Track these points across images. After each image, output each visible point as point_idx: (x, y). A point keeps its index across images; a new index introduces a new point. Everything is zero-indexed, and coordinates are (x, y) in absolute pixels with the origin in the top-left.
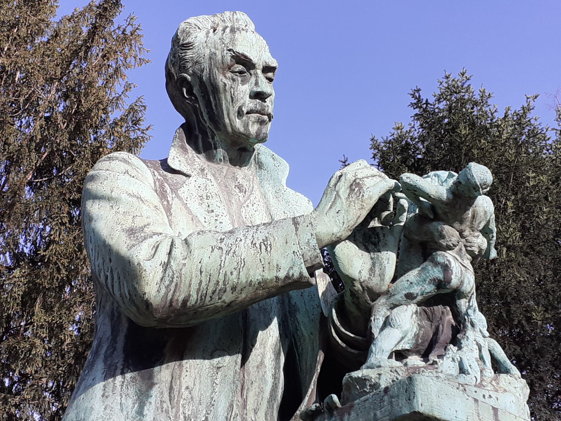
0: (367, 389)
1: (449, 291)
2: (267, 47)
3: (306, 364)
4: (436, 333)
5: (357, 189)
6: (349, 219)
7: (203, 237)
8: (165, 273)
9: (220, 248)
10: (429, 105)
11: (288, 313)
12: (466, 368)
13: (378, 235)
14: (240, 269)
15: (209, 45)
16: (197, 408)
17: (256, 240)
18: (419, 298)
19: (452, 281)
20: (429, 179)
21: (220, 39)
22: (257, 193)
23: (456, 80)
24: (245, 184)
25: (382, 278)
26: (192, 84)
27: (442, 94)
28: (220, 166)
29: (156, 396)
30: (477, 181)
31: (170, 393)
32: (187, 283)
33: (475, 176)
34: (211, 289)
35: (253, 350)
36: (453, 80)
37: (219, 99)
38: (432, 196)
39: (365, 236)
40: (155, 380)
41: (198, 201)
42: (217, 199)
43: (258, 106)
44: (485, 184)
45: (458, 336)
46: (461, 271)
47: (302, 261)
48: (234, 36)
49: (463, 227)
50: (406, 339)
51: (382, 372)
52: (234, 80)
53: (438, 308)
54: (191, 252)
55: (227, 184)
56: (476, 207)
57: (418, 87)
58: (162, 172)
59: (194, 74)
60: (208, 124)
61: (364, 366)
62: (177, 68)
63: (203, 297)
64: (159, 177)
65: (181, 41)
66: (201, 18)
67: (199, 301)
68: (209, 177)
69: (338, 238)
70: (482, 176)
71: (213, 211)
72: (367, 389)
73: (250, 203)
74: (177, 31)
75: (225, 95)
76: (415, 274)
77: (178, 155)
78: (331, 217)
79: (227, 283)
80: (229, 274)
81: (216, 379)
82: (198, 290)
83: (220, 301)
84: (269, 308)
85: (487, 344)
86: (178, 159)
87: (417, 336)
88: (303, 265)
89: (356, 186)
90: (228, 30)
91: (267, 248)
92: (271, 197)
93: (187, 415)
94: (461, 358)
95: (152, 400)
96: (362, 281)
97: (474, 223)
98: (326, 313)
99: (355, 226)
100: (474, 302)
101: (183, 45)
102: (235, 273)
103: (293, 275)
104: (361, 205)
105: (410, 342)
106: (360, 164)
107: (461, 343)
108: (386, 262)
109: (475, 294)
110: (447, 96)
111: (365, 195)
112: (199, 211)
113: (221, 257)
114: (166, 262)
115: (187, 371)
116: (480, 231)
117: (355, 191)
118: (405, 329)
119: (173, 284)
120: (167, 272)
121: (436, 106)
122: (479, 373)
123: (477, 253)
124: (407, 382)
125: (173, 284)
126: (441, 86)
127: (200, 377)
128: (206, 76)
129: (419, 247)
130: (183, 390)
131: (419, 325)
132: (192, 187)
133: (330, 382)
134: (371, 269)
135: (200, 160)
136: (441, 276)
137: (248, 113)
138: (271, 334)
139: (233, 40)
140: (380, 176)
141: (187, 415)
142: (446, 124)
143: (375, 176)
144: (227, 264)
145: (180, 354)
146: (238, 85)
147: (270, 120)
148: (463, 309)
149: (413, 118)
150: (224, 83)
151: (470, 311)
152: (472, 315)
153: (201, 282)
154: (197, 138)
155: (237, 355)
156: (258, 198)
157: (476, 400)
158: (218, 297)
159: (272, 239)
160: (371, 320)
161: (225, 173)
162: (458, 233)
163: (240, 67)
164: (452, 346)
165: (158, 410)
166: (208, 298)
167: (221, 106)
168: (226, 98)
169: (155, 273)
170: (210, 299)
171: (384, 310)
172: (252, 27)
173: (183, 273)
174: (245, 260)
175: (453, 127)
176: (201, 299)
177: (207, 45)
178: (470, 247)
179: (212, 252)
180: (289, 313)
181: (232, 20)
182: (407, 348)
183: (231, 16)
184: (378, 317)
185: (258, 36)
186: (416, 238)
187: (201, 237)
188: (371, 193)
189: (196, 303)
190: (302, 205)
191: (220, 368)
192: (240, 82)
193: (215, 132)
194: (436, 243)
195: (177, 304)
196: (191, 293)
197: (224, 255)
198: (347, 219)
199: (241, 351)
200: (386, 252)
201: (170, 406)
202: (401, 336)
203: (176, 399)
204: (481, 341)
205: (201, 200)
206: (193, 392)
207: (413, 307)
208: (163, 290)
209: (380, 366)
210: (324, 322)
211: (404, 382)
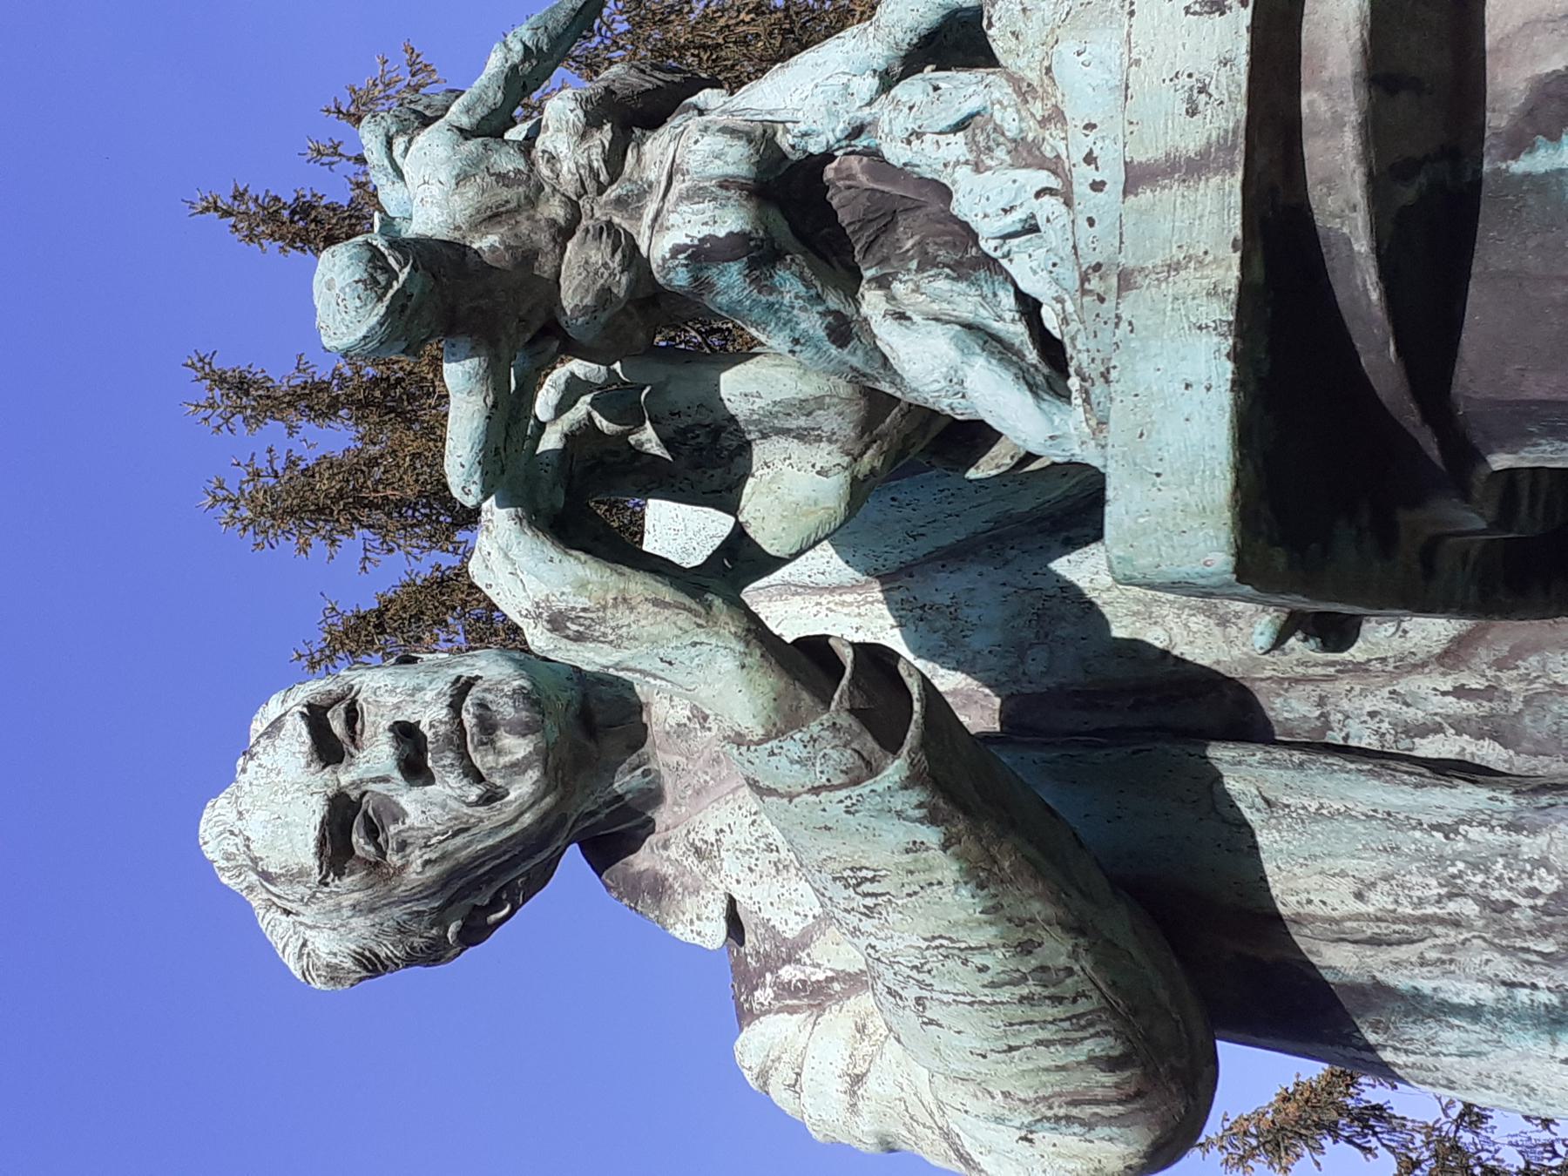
1: (774, 215)
14: (961, 950)
15: (338, 922)
16: (1413, 859)
18: (833, 301)
19: (736, 228)
25: (812, 405)
28: (664, 771)
30: (374, 320)
31: (1390, 944)
32: (1057, 1077)
34: (1052, 1012)
38: (490, 401)
43: (447, 762)
49: (543, 239)
50: (985, 317)
52: (403, 846)
56: (458, 228)
63: (1083, 1022)
67: (1099, 1028)
69: (747, 644)
75: (458, 850)
79: (1017, 975)
80: (986, 978)
81: (1304, 808)
82: (1066, 1042)
83: (1077, 968)
84: (1028, 598)
91: (866, 879)
93: (1443, 891)
95: (1426, 986)
96: (847, 459)
97: (512, 205)
102: (978, 960)
103: (920, 806)
104: (615, 606)
105: (987, 290)
108: (759, 403)
115: (1310, 902)
119: (1075, 1112)
125: (1075, 1112)
127: (1314, 857)
129: (666, 328)
130: (1371, 909)
131: (921, 269)
132: (759, 893)
137: (478, 778)
141: (1443, 891)
146: (410, 828)
153: (1039, 1043)
158: (1069, 981)
163: (358, 840)
166: (1083, 1006)
168: (466, 846)
169: (1059, 1155)
170: (1081, 1001)
173: (1032, 1095)
174: (928, 935)
176: (1091, 1024)
179: (940, 1026)
188: (567, 589)
189: (1106, 1033)
191: (1267, 801)
192: (401, 827)
195: (1125, 1081)
196: (1082, 1058)
197: (936, 995)
201: (1429, 942)
203: (1403, 927)
206: (1368, 877)
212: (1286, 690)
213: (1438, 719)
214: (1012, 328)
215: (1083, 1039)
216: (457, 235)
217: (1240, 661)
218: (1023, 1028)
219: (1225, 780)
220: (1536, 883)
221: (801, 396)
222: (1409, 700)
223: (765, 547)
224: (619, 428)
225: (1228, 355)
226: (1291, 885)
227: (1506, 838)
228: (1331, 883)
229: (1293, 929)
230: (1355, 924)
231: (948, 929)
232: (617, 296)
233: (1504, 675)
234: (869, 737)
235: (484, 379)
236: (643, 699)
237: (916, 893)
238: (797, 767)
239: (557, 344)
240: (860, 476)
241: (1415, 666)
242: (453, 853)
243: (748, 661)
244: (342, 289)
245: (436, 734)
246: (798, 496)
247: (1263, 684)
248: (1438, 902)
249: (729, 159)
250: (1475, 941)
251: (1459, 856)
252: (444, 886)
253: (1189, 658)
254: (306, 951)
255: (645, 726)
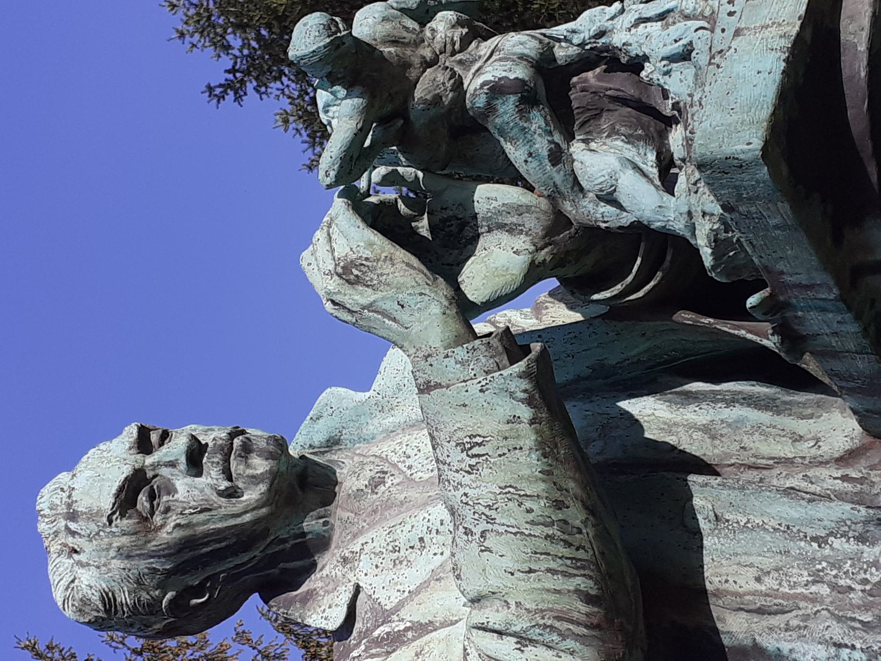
0: (733, 237)
1: (540, 82)
2: (102, 446)
3: (702, 342)
4: (624, 102)
5: (355, 272)
6: (414, 283)
7: (464, 569)
8: (537, 642)
9: (483, 534)
10: (237, 67)
11: (610, 381)
12: (681, 49)
13: (444, 221)
14: (519, 495)
15: (103, 560)
16: (796, 559)
17: (463, 466)
18: (557, 138)
19: (520, 76)
20: (334, 122)
21: (91, 541)
22: (385, 448)
23: (185, 18)
24: (369, 474)
26: (181, 588)
27: (214, 44)
28: (337, 524)
29: (777, 640)
30: (322, 44)
31: (769, 614)
32: (552, 597)
33: (314, 48)
35: (681, 448)
36: (186, 23)
37: (207, 535)
38: (359, 126)
39: (444, 248)
40: (748, 642)
41: (403, 570)
42: (399, 531)
43: (216, 460)
44: (329, 28)
45: (624, 60)
46: (500, 60)
47: (496, 374)
48: (83, 513)
49: (416, 61)
50: (638, 160)
51: (699, 209)
52: (168, 510)
53: (575, 99)
54: (493, 593)
55: (370, 509)
56: (375, 40)
57: (205, 89)
58: (352, 640)
59: (163, 587)
60: (257, 553)
61: (693, 242)
62: (153, 619)
63: (579, 564)
64: (363, 647)
65: (101, 614)
66: (53, 578)
67: (586, 572)
68: (357, 548)
69: (451, 304)
70: (313, 34)
71: (421, 540)
72: (733, 237)
73: (404, 462)
74: (82, 623)
75: (198, 524)
76: (513, 149)
77: (319, 610)
78: (413, 318)
79: (548, 520)
80: (530, 517)
81: (738, 522)
82: (565, 574)
83: (584, 531)
85: (634, 7)
86: (327, 610)
87: (630, 139)
88: (505, 373)
89: (350, 273)
90: (73, 526)
92: (391, 419)
93: (810, 579)
94: (663, 59)
95: (785, 647)
96: (533, 248)
97: (407, 41)
98: (603, 309)
99: (425, 271)
100: (560, 30)
101: (107, 611)
102: (528, 504)
103: (525, 391)
104: (385, 261)
105: (642, 151)
106: (309, 264)
107: (637, 55)
108: (495, 204)
109: (543, 31)
110: (216, 34)
111: (365, 256)
112: (423, 565)
113: (499, 534)
114: (515, 640)
116: (423, 25)
117: (359, 274)
118: (617, 165)
119: (557, 624)
120: (535, 638)
121: (238, 53)
122: (689, 23)
123: (465, 31)
124: (708, 172)
125: (557, 624)
126: (199, 45)
128: (163, 564)
129: (459, 143)
130: (763, 588)
131: (608, 136)
132: (377, 582)
133: (726, 300)
134: (511, 231)
135: (328, 565)
136: (512, 99)
137: (229, 478)
138: (651, 412)
139: (91, 516)
140: (329, 226)
141: (810, 579)
142: (271, 32)
143: (329, 235)
144: (512, 520)
145: (695, 595)
146: (176, 501)
147: (243, 432)
148: (573, 51)
149: (264, 96)
150: (174, 528)
151: (576, 41)
152: (582, 36)
153: (549, 570)
154: (284, 571)
155: (690, 484)
156: (393, 445)
157: (738, 33)
158: (577, 535)
159: (460, 434)
160: (606, 227)
161: (349, 514)
162: (428, 70)
163: (142, 498)
164: (643, 74)
165: (805, 636)
166: (581, 554)
167: (219, 531)
168: (204, 523)
170: (581, 551)
171: (585, 204)
172: (63, 478)
173: (534, 607)
174: (503, 485)
175: (275, 19)
176: (583, 568)
177: (105, 565)
178: (454, 44)
179: (491, 552)
180: (607, 378)
181: (53, 518)
182: (654, 158)
183: (46, 520)
184: (599, 216)
185: (80, 466)
186: (444, 148)
187: (465, 572)
188: (362, 244)
189: (591, 578)
190: (395, 365)
191: (716, 516)
192: (171, 498)
193: (273, 538)
194: (450, 110)
196: (572, 588)
198: (413, 286)
199: (683, 476)
200: (476, 204)
201: (794, 613)
202: (631, 172)
203: (781, 601)
204: (629, 18)
205: (401, 562)
207: (577, 149)
208: (570, 643)
209: (689, 213)
210: (616, 311)
211: (708, 177)
212: (742, 473)
213: (828, 492)
214: (650, 169)
215: (575, 575)
216: (374, 42)
217: (718, 456)
218: (543, 556)
219: (694, 499)
220: (868, 576)
221: (519, 203)
222: (814, 480)
223: (469, 296)
224: (410, 212)
225: (784, 60)
226: (717, 570)
227: (856, 547)
228: (743, 571)
229: (712, 600)
230: (751, 598)
231: (517, 481)
232: (443, 103)
233: (873, 473)
234: (506, 358)
235: (361, 112)
236: (339, 480)
237: (504, 454)
238: (459, 366)
239: (402, 122)
240: (536, 262)
241: (821, 463)
242: (194, 525)
243: (448, 312)
244: (311, 27)
245: (215, 444)
246: (498, 264)
247: (729, 469)
248: (806, 585)
249: (527, 46)
250: (824, 612)
251: (825, 558)
252: (179, 551)
253: (688, 451)
254: (72, 585)
255: (335, 494)
